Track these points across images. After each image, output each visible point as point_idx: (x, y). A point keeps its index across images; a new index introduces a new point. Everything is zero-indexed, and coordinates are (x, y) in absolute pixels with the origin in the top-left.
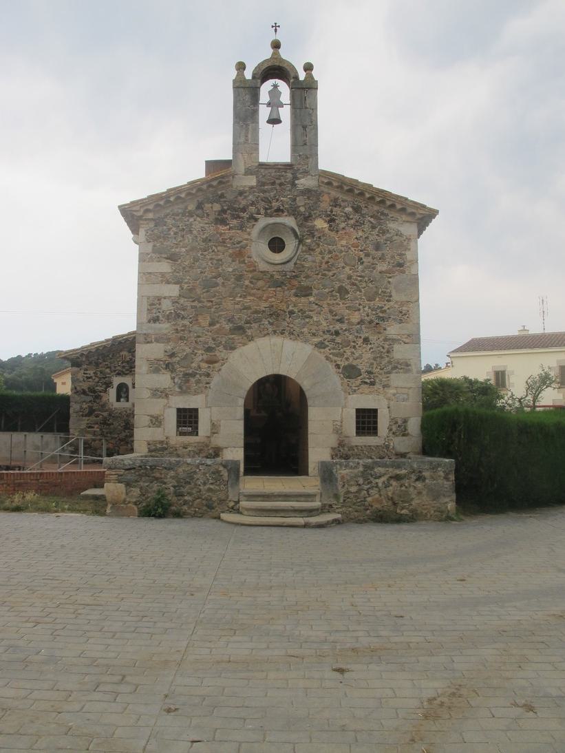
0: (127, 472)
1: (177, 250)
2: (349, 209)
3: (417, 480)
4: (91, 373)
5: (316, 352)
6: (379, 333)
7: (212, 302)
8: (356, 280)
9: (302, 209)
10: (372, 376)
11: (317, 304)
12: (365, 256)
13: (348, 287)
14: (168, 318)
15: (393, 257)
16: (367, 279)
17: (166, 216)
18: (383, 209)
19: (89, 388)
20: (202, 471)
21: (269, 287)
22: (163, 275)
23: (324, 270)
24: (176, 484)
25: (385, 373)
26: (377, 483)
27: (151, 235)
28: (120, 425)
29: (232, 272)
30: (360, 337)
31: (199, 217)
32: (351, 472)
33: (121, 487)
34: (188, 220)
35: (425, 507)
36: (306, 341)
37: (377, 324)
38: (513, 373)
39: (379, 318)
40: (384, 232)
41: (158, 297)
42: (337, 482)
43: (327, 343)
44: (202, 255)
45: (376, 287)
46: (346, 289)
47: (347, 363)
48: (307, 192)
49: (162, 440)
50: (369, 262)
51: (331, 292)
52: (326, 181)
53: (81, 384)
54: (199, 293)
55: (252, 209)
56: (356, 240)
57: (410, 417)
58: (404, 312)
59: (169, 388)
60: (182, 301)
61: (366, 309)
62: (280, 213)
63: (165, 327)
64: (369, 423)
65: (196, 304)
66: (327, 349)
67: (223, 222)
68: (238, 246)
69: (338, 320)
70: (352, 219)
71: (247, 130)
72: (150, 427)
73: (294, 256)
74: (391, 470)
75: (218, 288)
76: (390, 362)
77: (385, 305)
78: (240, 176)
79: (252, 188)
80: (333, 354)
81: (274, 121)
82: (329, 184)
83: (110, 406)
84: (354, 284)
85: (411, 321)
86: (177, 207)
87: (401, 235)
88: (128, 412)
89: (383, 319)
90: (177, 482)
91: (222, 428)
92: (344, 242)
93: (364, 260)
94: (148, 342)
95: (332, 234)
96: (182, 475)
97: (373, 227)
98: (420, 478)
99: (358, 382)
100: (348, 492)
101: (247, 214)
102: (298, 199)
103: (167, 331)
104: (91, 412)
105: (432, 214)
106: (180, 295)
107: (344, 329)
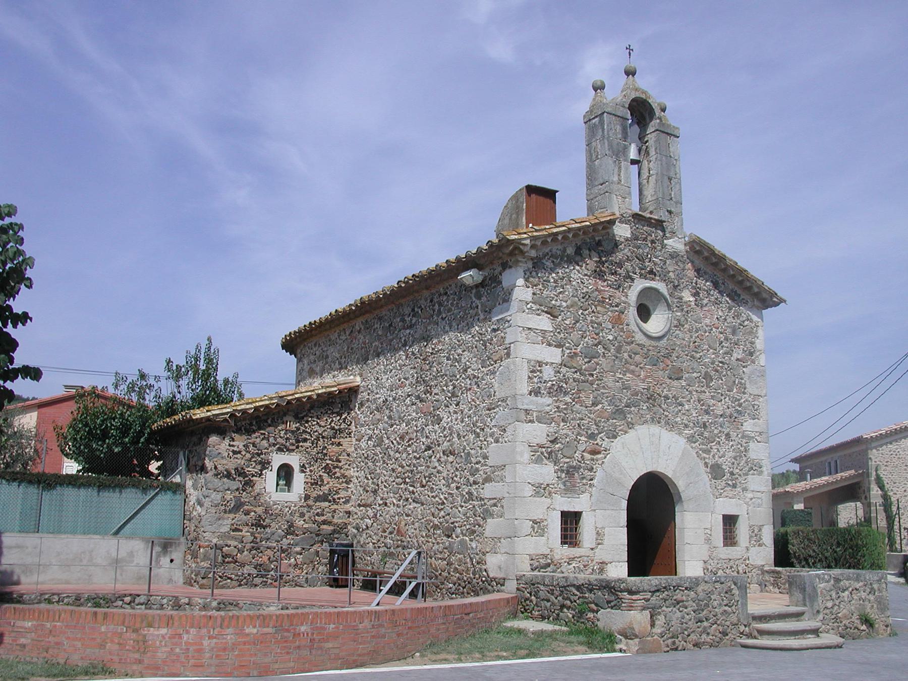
8: (718, 366)
19: (236, 469)
24: (696, 608)
28: (280, 528)
36: (680, 434)
39: (738, 411)
44: (582, 314)
53: (225, 462)
60: (564, 370)
63: (545, 402)
66: (697, 444)
79: (627, 240)
80: (704, 451)
83: (267, 498)
84: (717, 371)
90: (698, 605)
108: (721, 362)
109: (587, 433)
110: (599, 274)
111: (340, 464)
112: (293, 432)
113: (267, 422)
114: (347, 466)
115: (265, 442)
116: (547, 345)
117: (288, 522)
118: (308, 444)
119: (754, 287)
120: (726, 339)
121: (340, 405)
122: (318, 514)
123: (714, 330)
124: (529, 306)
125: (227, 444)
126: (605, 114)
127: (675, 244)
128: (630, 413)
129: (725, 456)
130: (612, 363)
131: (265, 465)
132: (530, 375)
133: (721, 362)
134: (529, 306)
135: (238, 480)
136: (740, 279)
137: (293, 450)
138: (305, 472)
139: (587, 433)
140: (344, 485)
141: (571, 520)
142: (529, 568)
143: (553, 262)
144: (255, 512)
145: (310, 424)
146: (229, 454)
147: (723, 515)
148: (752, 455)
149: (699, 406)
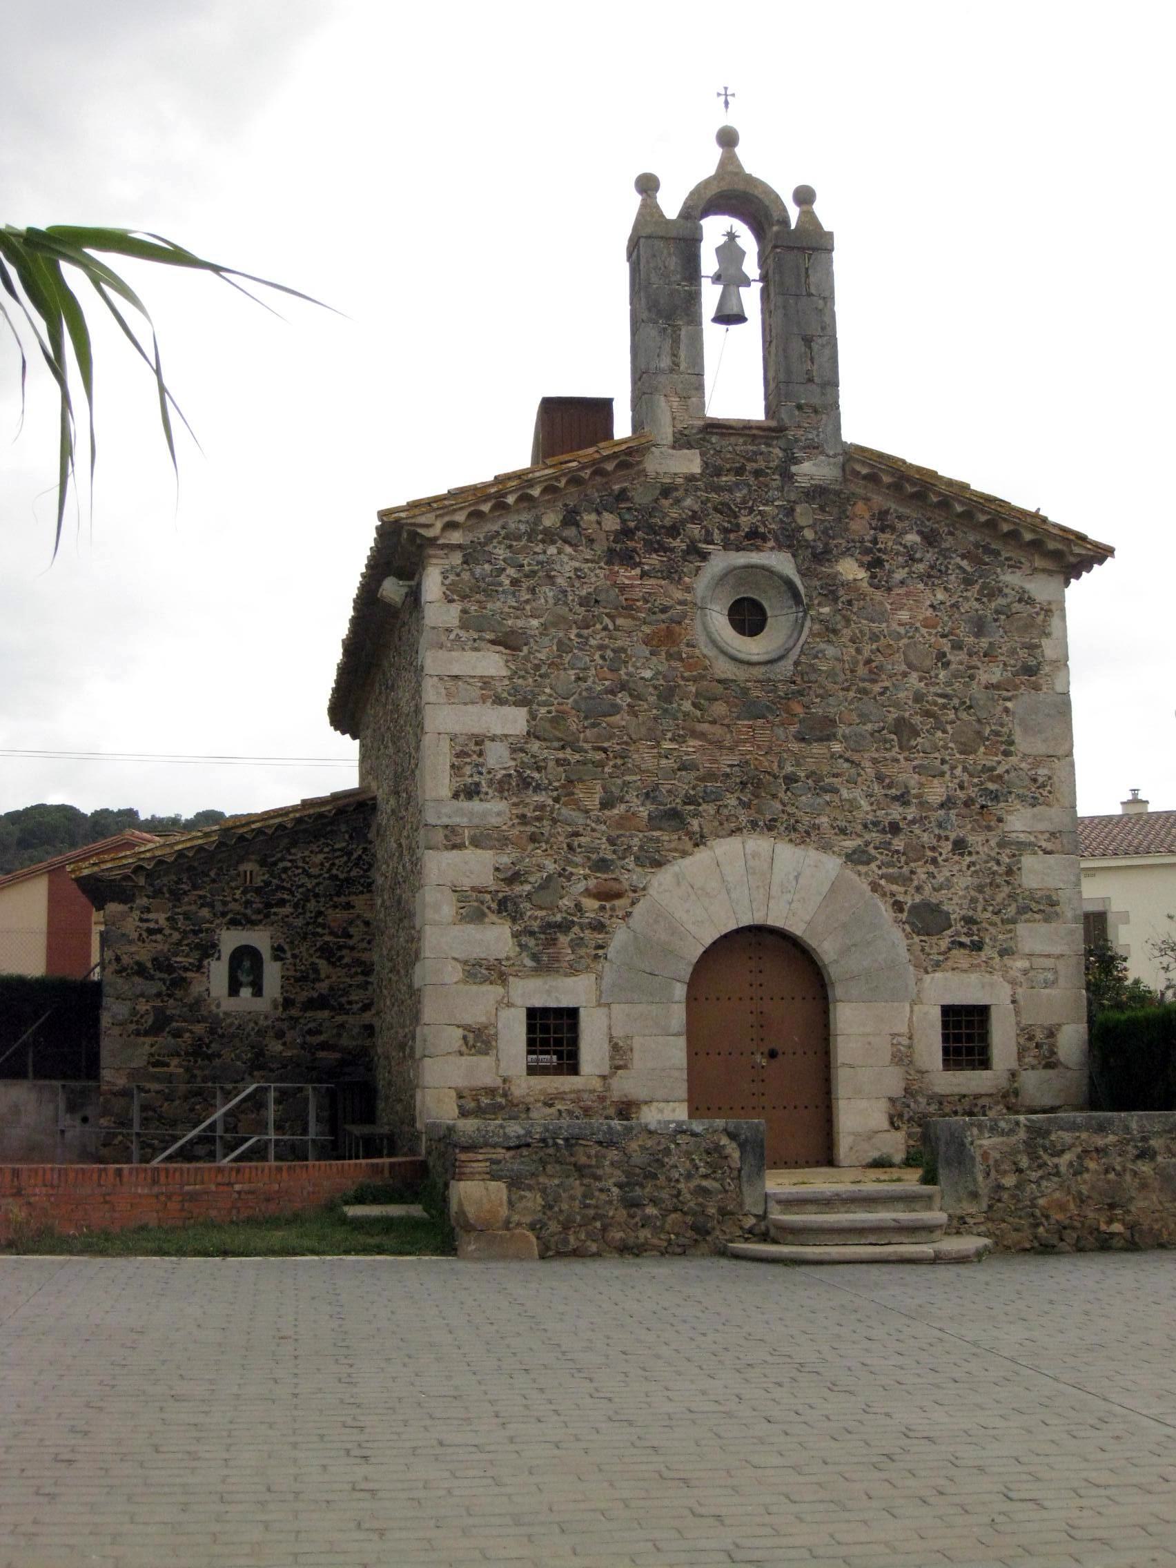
0: (511, 1153)
1: (520, 623)
2: (912, 538)
3: (1138, 1157)
4: (161, 918)
5: (849, 873)
6: (989, 828)
7: (605, 750)
8: (935, 704)
9: (809, 534)
10: (975, 928)
11: (847, 760)
12: (953, 648)
13: (917, 720)
14: (502, 787)
15: (1013, 652)
16: (956, 702)
17: (490, 539)
18: (988, 540)
19: (154, 960)
20: (684, 1147)
21: (738, 718)
22: (486, 682)
23: (863, 680)
24: (623, 1179)
25: (1003, 921)
26: (1056, 1166)
27: (453, 583)
28: (238, 1058)
29: (652, 679)
30: (947, 839)
31: (571, 545)
32: (1002, 1143)
33: (498, 1189)
34: (545, 552)
35: (1157, 1215)
36: (826, 847)
37: (983, 807)
38: (1125, 917)
40: (992, 592)
41: (477, 736)
42: (974, 1166)
43: (873, 852)
44: (578, 636)
45: (979, 721)
46: (911, 723)
47: (918, 898)
48: (817, 493)
50: (961, 663)
51: (879, 732)
52: (865, 471)
54: (574, 727)
55: (695, 530)
56: (930, 610)
57: (1060, 1025)
58: (1041, 780)
59: (508, 959)
60: (535, 746)
61: (958, 771)
62: (759, 542)
64: (970, 1038)
65: (568, 754)
66: (873, 866)
67: (628, 559)
68: (663, 616)
69: (896, 798)
70: (921, 560)
71: (676, 341)
72: (461, 1054)
73: (795, 645)
74: (1084, 1135)
75: (618, 717)
76: (1012, 897)
77: (999, 763)
78: (664, 449)
79: (691, 478)
80: (891, 879)
81: (730, 317)
82: (873, 478)
83: (213, 1008)
84: (928, 714)
85: (1058, 800)
86: (516, 518)
87: (1030, 601)
88: (262, 1022)
89: (995, 797)
90: (628, 1174)
91: (636, 1055)
92: (904, 616)
93: (949, 657)
94: (455, 847)
95: (878, 595)
96: (638, 1159)
97: (968, 582)
98: (1145, 1154)
99: (944, 944)
100: (1000, 1187)
101: (682, 541)
102: (798, 509)
103: (499, 819)
104: (160, 1024)
105: (1101, 553)
106: (528, 733)
107: (909, 817)
111: (351, 942)
113: (208, 875)
114: (365, 945)
116: (494, 702)
117: (253, 1047)
118: (287, 910)
119: (1022, 530)
121: (347, 836)
122: (310, 1032)
125: (137, 918)
126: (642, 241)
128: (696, 815)
131: (208, 950)
132: (457, 762)
134: (452, 636)
135: (160, 979)
140: (361, 978)
144: (191, 1032)
145: (290, 873)
146: (140, 935)
147: (943, 1006)
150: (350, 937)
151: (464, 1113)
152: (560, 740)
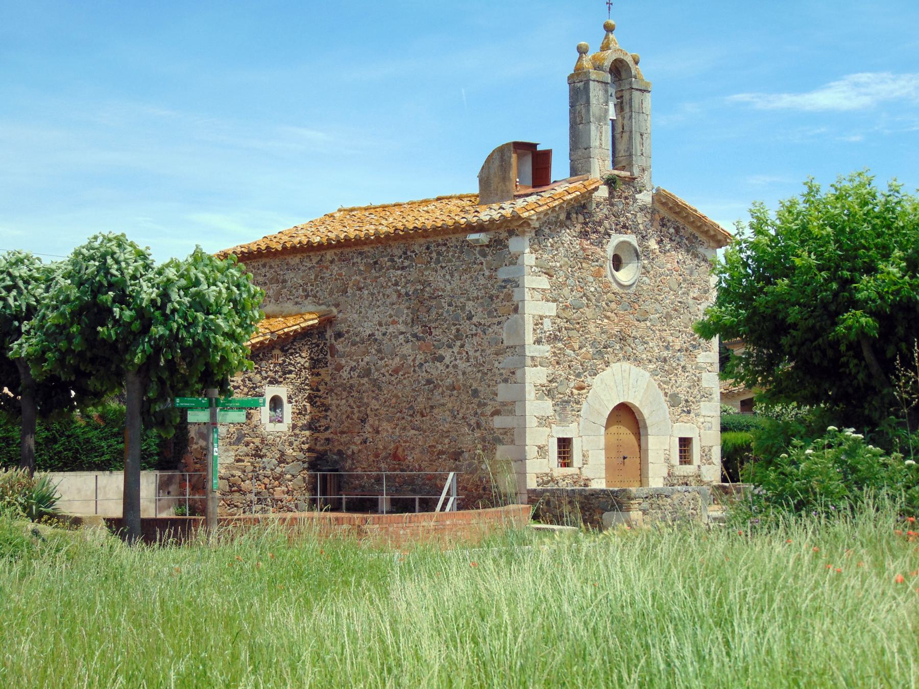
36: (645, 369)
49: (547, 472)
60: (558, 321)
66: (659, 377)
80: (665, 383)
99: (679, 410)
108: (680, 302)
109: (575, 372)
110: (584, 235)
111: (320, 394)
112: (280, 365)
115: (258, 376)
118: (293, 376)
120: (685, 280)
123: (675, 273)
124: (533, 270)
127: (645, 198)
129: (682, 385)
130: (594, 312)
132: (535, 327)
133: (680, 302)
136: (699, 224)
137: (281, 382)
138: (291, 403)
139: (575, 372)
140: (324, 413)
141: (564, 445)
142: (536, 484)
143: (550, 228)
144: (254, 443)
148: (704, 384)
149: (661, 344)
150: (319, 391)
151: (538, 486)
152: (566, 318)
